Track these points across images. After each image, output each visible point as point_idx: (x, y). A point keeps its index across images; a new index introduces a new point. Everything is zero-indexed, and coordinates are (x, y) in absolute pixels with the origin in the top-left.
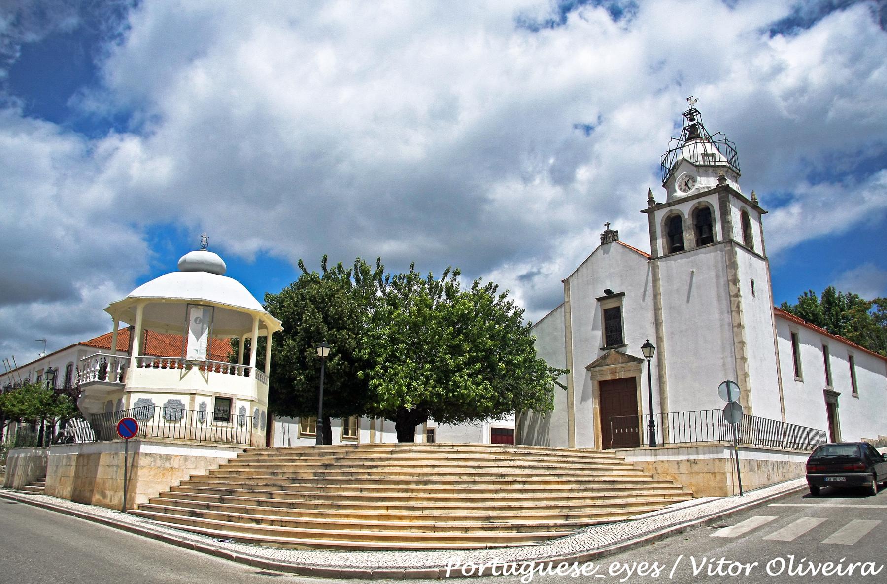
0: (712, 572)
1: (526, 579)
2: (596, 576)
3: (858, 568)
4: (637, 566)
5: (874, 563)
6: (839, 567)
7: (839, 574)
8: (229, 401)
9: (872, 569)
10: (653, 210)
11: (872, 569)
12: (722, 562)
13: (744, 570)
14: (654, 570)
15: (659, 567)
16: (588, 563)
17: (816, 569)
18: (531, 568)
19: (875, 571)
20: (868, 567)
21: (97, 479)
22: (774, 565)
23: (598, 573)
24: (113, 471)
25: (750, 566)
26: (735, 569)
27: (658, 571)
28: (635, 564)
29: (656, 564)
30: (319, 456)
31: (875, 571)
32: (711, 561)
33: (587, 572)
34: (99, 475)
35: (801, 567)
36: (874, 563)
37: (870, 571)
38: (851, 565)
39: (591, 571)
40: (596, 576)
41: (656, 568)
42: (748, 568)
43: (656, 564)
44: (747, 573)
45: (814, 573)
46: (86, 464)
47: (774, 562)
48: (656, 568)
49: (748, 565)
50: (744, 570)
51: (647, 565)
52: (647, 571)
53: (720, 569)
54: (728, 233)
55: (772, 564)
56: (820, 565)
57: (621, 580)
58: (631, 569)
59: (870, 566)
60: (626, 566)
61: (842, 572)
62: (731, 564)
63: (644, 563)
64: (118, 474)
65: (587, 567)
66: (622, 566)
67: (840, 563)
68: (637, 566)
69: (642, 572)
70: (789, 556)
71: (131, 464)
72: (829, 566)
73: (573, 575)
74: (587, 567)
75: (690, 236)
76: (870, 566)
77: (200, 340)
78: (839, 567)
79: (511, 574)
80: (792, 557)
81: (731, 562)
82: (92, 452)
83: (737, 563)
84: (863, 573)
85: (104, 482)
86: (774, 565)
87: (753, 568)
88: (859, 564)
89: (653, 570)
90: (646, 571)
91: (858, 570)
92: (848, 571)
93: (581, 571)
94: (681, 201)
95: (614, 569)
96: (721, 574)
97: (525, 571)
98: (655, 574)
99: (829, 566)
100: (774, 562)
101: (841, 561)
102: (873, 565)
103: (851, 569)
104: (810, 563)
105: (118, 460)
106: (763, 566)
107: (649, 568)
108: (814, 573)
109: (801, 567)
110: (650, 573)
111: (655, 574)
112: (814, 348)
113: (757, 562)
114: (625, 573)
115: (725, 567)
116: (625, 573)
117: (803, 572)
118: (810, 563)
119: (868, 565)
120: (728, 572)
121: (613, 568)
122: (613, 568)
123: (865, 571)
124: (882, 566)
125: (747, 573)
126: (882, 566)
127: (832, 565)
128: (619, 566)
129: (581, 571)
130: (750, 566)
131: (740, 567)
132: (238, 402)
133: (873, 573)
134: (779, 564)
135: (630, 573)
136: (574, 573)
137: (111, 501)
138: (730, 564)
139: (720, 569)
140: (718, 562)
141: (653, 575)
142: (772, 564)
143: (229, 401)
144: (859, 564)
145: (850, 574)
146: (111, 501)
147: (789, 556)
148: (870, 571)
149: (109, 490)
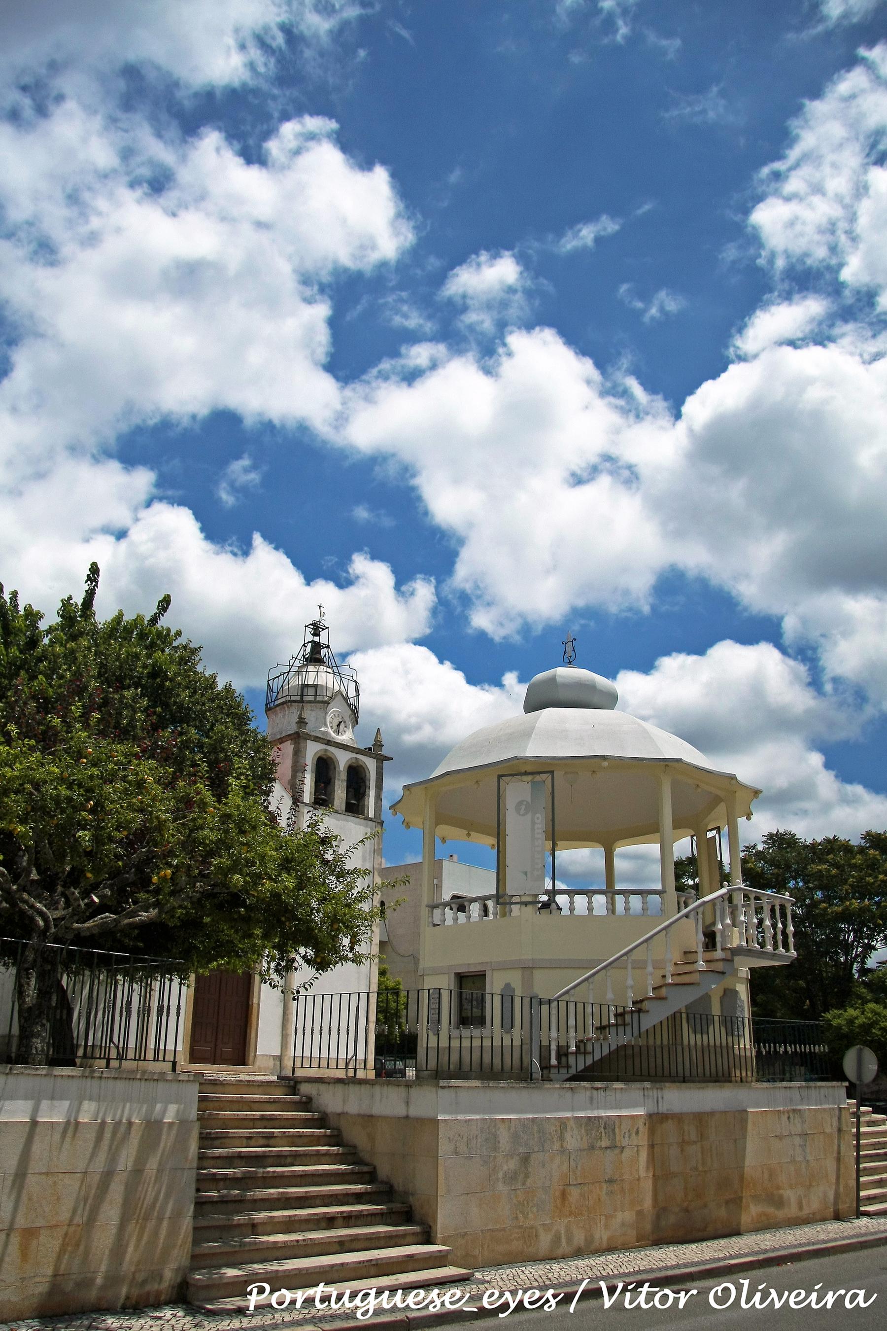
0: (630, 1304)
3: (842, 1298)
4: (789, 1296)
5: (863, 1291)
6: (814, 1296)
7: (814, 1306)
8: (480, 977)
9: (860, 1299)
11: (860, 1299)
12: (646, 1288)
13: (677, 1300)
14: (548, 1301)
16: (417, 1291)
17: (780, 1299)
18: (372, 1297)
19: (865, 1302)
20: (855, 1296)
21: (746, 1169)
22: (719, 1294)
24: (794, 1145)
25: (686, 1295)
30: (271, 1136)
31: (865, 1302)
32: (630, 1287)
33: (796, 1303)
34: (750, 1161)
35: (758, 1296)
36: (863, 1291)
37: (858, 1303)
38: (831, 1293)
39: (459, 1300)
41: (551, 1298)
42: (683, 1299)
45: (778, 1305)
46: (693, 1136)
47: (720, 1288)
48: (551, 1298)
52: (421, 1303)
53: (642, 1299)
56: (786, 1293)
57: (501, 1315)
60: (508, 1295)
61: (817, 1304)
63: (493, 1290)
64: (808, 1150)
65: (416, 1296)
66: (501, 1295)
67: (759, 1291)
68: (789, 1296)
69: (796, 1303)
70: (741, 1281)
71: (836, 1129)
72: (799, 1294)
74: (416, 1296)
78: (814, 1296)
80: (746, 1283)
81: (657, 1289)
82: (708, 1108)
84: (848, 1306)
85: (772, 1174)
86: (719, 1294)
88: (842, 1292)
91: (840, 1300)
94: (341, 746)
96: (644, 1306)
97: (362, 1301)
99: (799, 1294)
100: (720, 1288)
101: (816, 1287)
102: (862, 1293)
103: (830, 1299)
104: (772, 1291)
105: (803, 1122)
106: (704, 1293)
108: (778, 1305)
109: (758, 1296)
111: (434, 1307)
112: (723, 375)
115: (650, 1297)
117: (761, 1304)
118: (772, 1291)
123: (851, 1303)
124: (876, 1295)
126: (876, 1295)
127: (803, 1293)
130: (686, 1295)
131: (672, 1296)
132: (496, 975)
133: (863, 1305)
134: (726, 1290)
135: (513, 1306)
136: (433, 1305)
137: (801, 1208)
138: (657, 1292)
139: (642, 1299)
140: (639, 1290)
141: (546, 1308)
143: (480, 977)
144: (842, 1292)
145: (829, 1306)
146: (801, 1208)
147: (741, 1281)
148: (858, 1303)
149: (791, 1187)
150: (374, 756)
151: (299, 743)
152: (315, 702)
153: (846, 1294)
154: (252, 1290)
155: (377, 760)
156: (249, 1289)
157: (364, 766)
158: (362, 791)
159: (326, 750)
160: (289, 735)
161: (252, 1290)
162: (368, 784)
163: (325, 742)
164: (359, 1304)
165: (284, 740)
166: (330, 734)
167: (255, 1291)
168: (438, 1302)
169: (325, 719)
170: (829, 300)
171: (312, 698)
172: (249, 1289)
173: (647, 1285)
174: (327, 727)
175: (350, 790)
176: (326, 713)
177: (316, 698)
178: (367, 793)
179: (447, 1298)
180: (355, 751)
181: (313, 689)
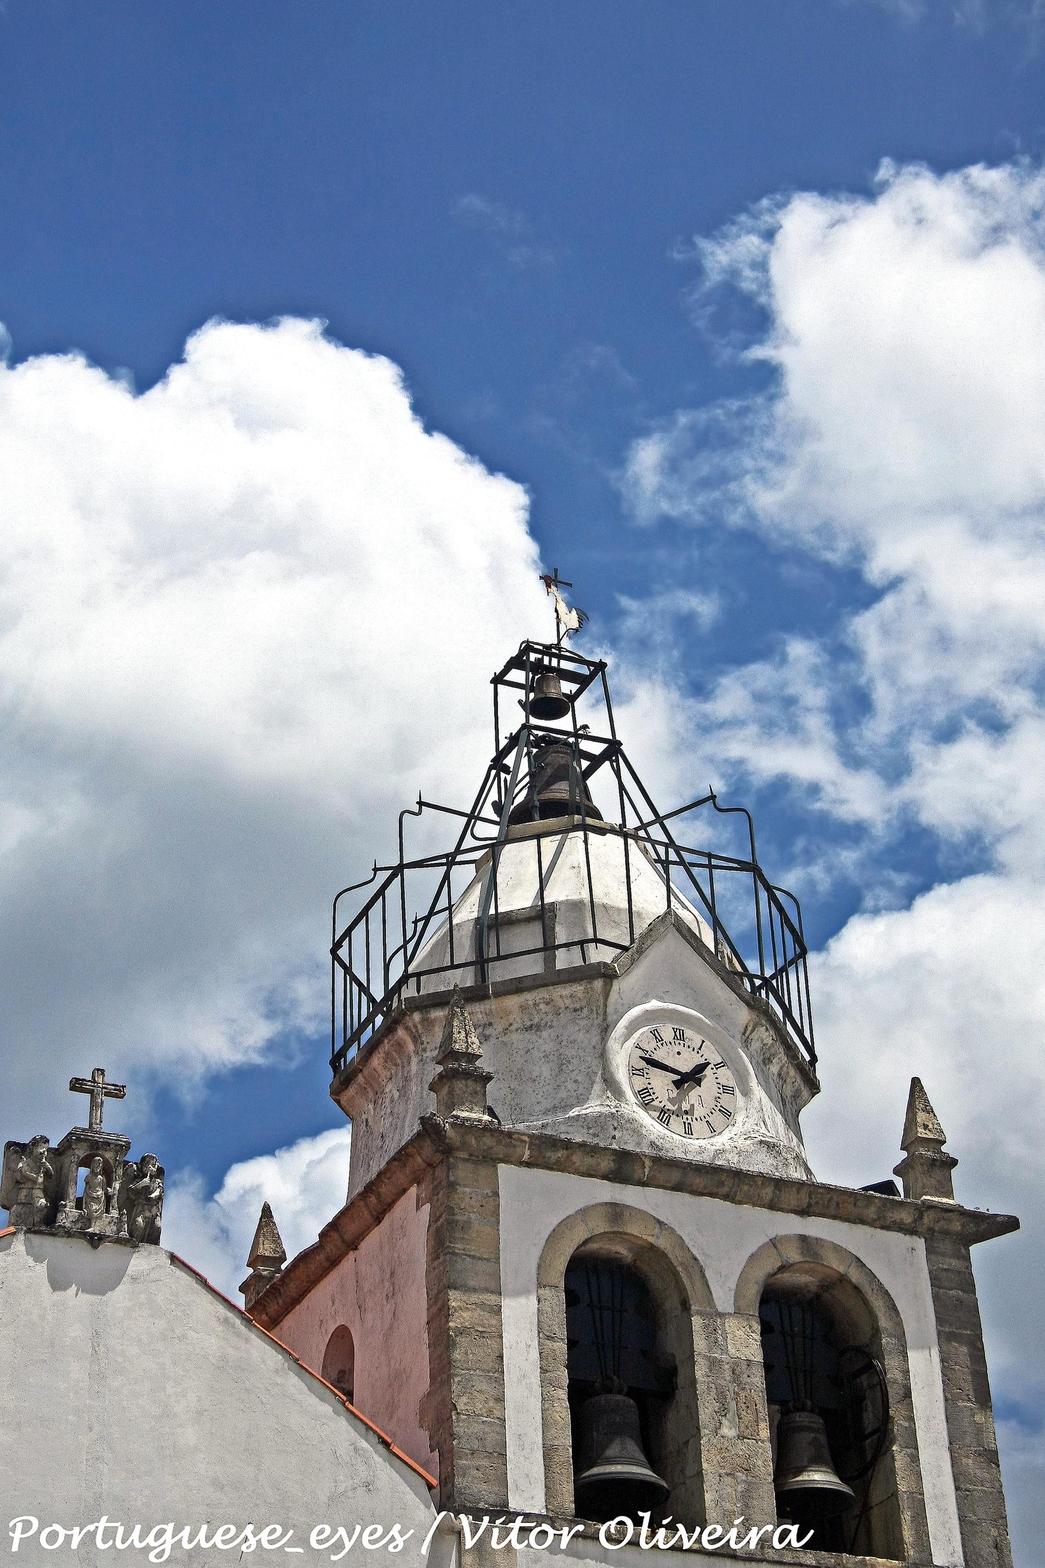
1: (160, 1555)
2: (287, 1549)
5: (797, 1527)
6: (733, 1534)
10: (500, 1150)
11: (793, 1536)
13: (69, 1538)
14: (393, 1539)
15: (402, 1533)
22: (613, 1531)
23: (288, 1544)
25: (81, 1530)
26: (53, 1537)
27: (400, 1541)
28: (358, 1528)
29: (397, 1527)
35: (662, 1532)
36: (797, 1527)
37: (790, 1542)
38: (755, 1529)
40: (287, 1549)
41: (397, 1536)
43: (397, 1527)
44: (74, 1545)
48: (397, 1536)
49: (77, 1529)
50: (69, 1538)
51: (380, 1530)
54: (751, 1202)
55: (609, 1528)
57: (333, 1558)
58: (473, 1536)
59: (790, 1531)
60: (342, 1531)
62: (535, 1527)
63: (373, 1527)
66: (334, 1531)
69: (371, 1542)
70: (640, 1514)
73: (244, 1548)
75: (741, 1447)
76: (790, 1531)
77: (570, 1308)
79: (656, 1547)
80: (646, 1516)
81: (534, 1524)
83: (56, 1527)
86: (613, 1531)
87: (573, 1536)
89: (391, 1538)
90: (232, 1539)
92: (749, 1542)
93: (259, 1542)
94: (698, 1181)
95: (372, 1538)
98: (396, 1547)
99: (228, 1530)
100: (613, 1523)
102: (794, 1529)
103: (754, 1536)
107: (237, 1536)
110: (240, 1545)
111: (396, 1547)
113: (771, 1523)
114: (339, 1546)
116: (339, 1546)
118: (680, 1526)
119: (785, 1529)
120: (529, 1543)
121: (223, 1536)
122: (223, 1536)
123: (781, 1541)
124: (812, 1532)
125: (74, 1545)
126: (812, 1532)
128: (328, 1530)
129: (259, 1542)
130: (81, 1530)
131: (62, 1533)
135: (348, 1545)
136: (247, 1544)
141: (391, 1548)
142: (609, 1528)
144: (91, 1528)
147: (640, 1514)
148: (790, 1542)
150: (906, 1217)
151: (452, 1186)
152: (553, 978)
153: (773, 1532)
154: (15, 1525)
155: (931, 1237)
156: (11, 1524)
157: (855, 1276)
158: (869, 1420)
159: (616, 1211)
160: (402, 1156)
161: (15, 1525)
162: (893, 1373)
163: (606, 1164)
164: (153, 1544)
165: (386, 1190)
166: (636, 1129)
167: (19, 1526)
168: (253, 1541)
169: (603, 1056)
170: (799, 720)
171: (530, 966)
172: (11, 1524)
173: (520, 1518)
174: (618, 1093)
175: (802, 1418)
176: (606, 1030)
177: (550, 961)
178: (899, 1423)
179: (264, 1536)
180: (791, 1198)
181: (537, 928)
